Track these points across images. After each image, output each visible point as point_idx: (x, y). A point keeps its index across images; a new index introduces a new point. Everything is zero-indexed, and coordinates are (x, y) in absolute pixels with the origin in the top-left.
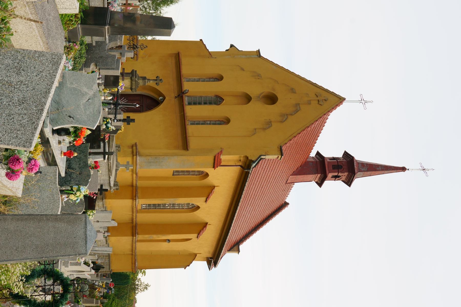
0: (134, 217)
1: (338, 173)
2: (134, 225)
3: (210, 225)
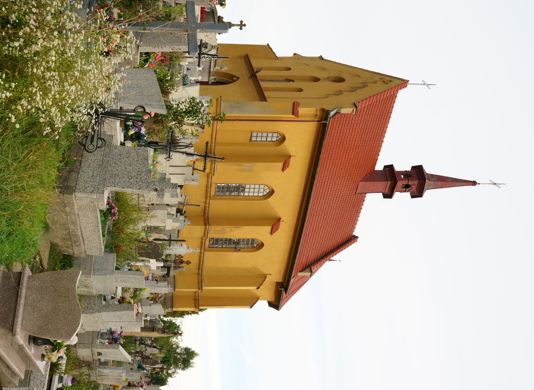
0: (207, 206)
1: (408, 181)
2: (206, 217)
3: (283, 221)
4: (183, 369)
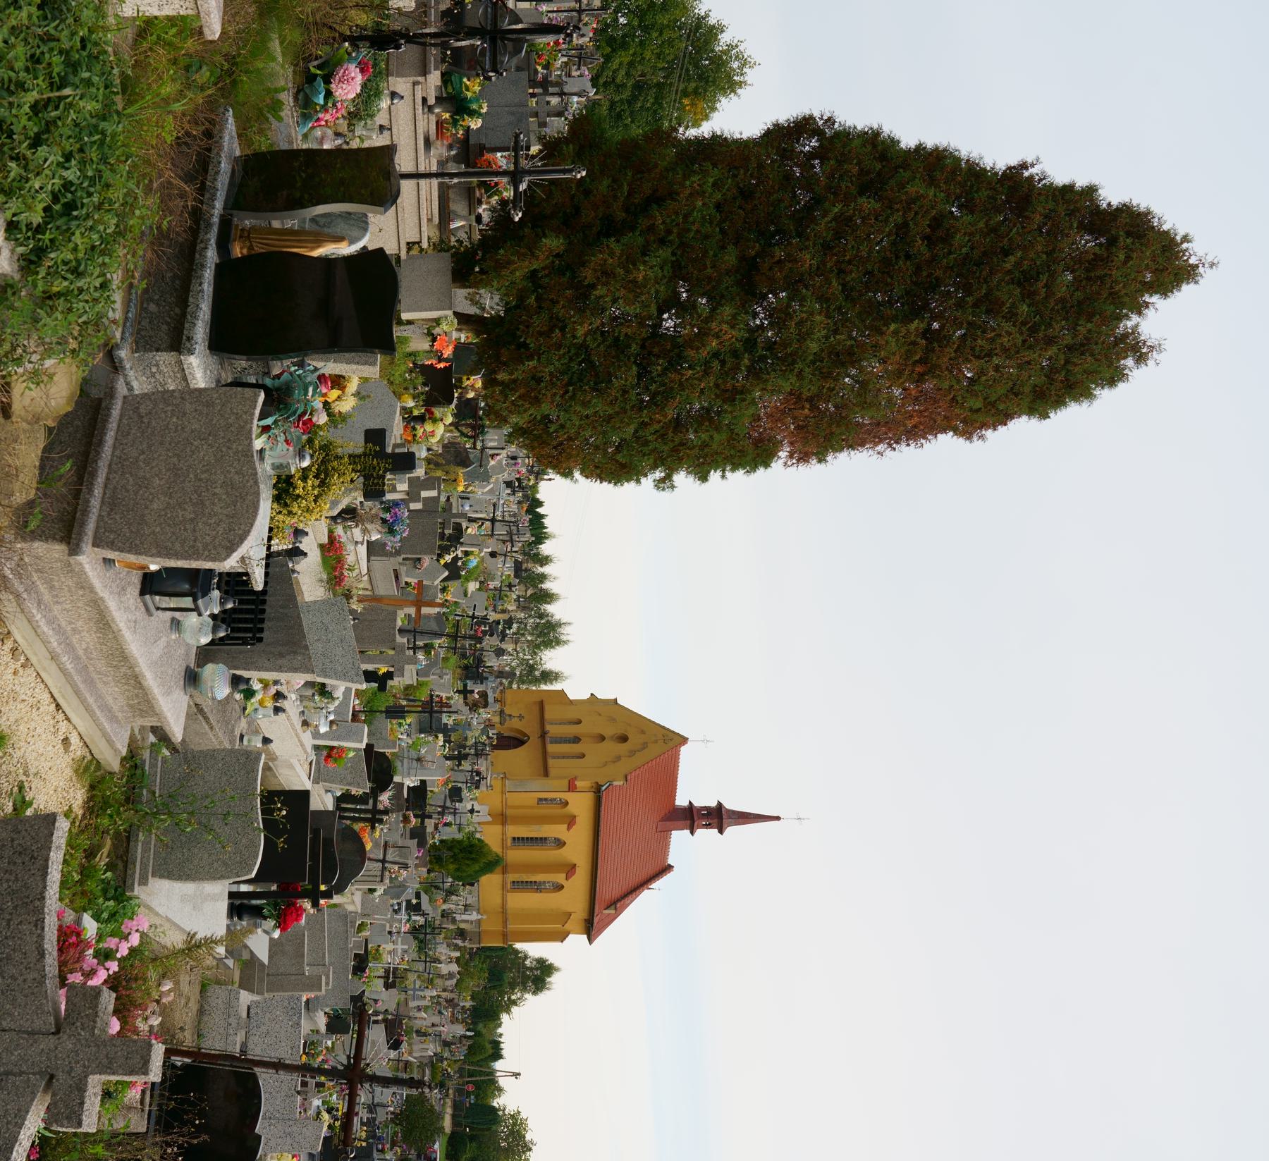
4: (535, 993)
